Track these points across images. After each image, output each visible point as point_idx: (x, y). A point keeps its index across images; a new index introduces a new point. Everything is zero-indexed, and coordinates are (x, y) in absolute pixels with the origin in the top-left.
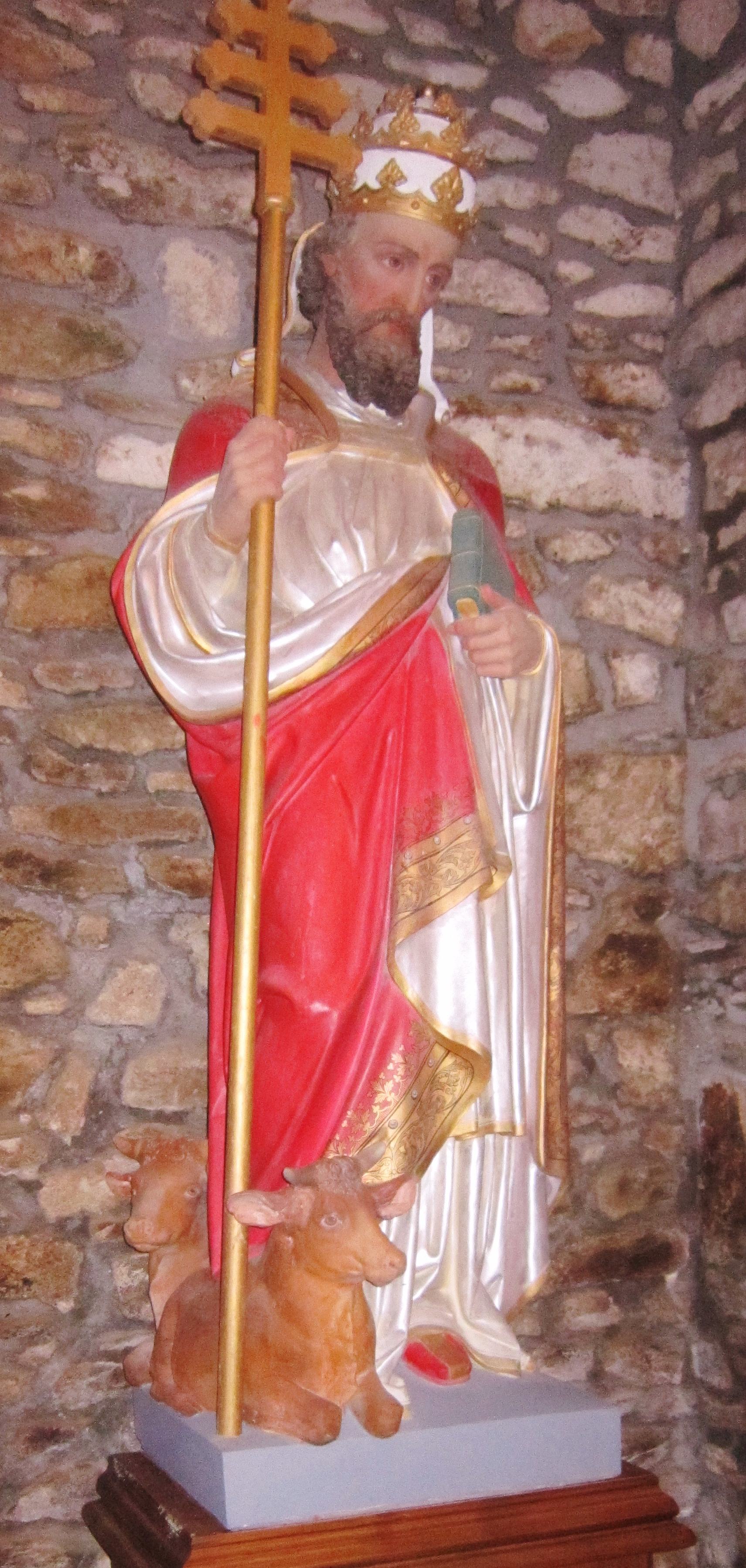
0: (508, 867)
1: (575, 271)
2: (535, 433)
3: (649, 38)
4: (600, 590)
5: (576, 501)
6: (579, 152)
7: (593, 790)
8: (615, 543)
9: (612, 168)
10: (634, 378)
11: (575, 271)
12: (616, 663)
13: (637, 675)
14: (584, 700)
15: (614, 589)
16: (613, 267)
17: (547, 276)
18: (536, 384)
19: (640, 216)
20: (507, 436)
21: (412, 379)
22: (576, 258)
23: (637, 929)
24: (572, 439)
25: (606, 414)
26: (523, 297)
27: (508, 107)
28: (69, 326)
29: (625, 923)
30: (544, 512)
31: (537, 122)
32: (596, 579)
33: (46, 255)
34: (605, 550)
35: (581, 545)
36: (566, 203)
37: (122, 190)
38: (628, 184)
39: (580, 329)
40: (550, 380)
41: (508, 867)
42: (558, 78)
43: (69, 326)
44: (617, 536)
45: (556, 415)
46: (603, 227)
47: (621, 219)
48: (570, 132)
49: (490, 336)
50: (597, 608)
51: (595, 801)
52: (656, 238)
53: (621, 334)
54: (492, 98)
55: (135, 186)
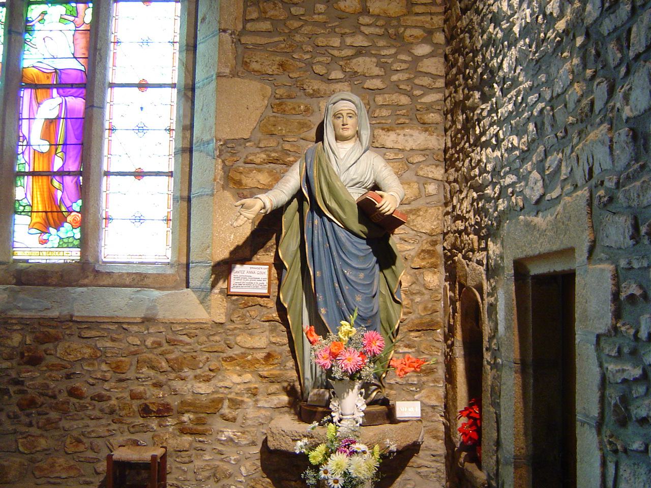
0: (15, 430)
1: (417, 92)
2: (406, 133)
3: (438, 34)
4: (422, 169)
5: (417, 148)
6: (420, 64)
7: (419, 216)
8: (427, 157)
9: (428, 67)
10: (432, 117)
11: (417, 92)
12: (425, 186)
13: (431, 188)
14: (417, 195)
15: (426, 168)
16: (429, 89)
17: (411, 95)
18: (407, 121)
19: (435, 77)
20: (399, 135)
21: (264, 457)
22: (418, 90)
23: (431, 248)
24: (416, 133)
25: (425, 126)
26: (404, 100)
27: (403, 57)
28: (299, 123)
29: (427, 247)
30: (409, 151)
31: (410, 59)
32: (422, 166)
33: (294, 109)
34: (424, 159)
35: (418, 159)
36: (415, 77)
37: (311, 92)
38: (433, 70)
39: (418, 107)
40: (411, 119)
41: (15, 430)
42: (414, 47)
43: (299, 123)
44: (428, 155)
45: (412, 128)
46: (426, 81)
47: (430, 79)
48: (418, 59)
49: (396, 111)
50: (421, 173)
51: (420, 218)
52: (439, 82)
53: (429, 108)
54: (391, 77)
55: (314, 90)
